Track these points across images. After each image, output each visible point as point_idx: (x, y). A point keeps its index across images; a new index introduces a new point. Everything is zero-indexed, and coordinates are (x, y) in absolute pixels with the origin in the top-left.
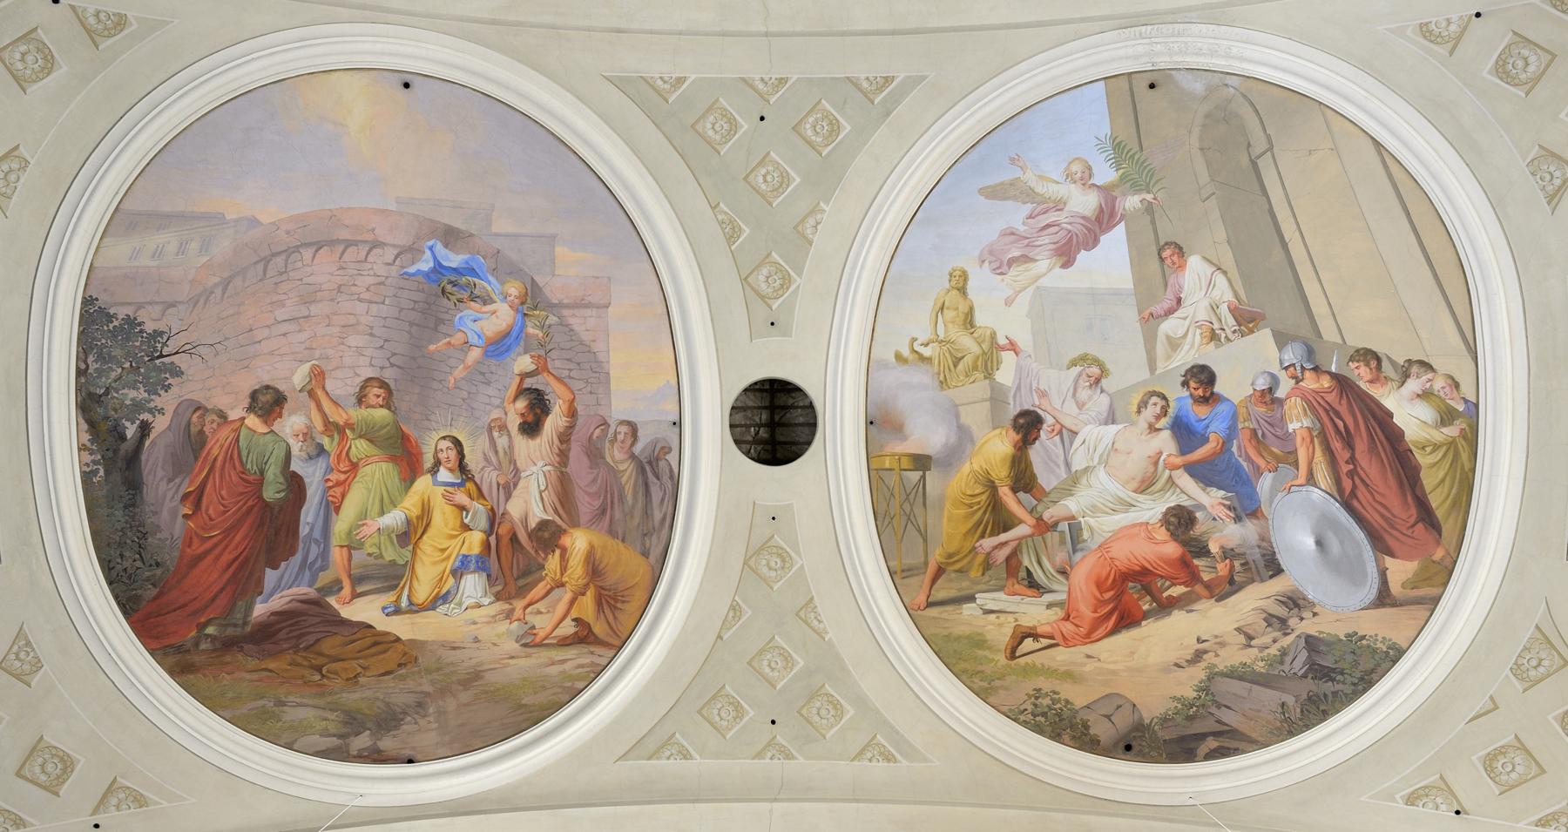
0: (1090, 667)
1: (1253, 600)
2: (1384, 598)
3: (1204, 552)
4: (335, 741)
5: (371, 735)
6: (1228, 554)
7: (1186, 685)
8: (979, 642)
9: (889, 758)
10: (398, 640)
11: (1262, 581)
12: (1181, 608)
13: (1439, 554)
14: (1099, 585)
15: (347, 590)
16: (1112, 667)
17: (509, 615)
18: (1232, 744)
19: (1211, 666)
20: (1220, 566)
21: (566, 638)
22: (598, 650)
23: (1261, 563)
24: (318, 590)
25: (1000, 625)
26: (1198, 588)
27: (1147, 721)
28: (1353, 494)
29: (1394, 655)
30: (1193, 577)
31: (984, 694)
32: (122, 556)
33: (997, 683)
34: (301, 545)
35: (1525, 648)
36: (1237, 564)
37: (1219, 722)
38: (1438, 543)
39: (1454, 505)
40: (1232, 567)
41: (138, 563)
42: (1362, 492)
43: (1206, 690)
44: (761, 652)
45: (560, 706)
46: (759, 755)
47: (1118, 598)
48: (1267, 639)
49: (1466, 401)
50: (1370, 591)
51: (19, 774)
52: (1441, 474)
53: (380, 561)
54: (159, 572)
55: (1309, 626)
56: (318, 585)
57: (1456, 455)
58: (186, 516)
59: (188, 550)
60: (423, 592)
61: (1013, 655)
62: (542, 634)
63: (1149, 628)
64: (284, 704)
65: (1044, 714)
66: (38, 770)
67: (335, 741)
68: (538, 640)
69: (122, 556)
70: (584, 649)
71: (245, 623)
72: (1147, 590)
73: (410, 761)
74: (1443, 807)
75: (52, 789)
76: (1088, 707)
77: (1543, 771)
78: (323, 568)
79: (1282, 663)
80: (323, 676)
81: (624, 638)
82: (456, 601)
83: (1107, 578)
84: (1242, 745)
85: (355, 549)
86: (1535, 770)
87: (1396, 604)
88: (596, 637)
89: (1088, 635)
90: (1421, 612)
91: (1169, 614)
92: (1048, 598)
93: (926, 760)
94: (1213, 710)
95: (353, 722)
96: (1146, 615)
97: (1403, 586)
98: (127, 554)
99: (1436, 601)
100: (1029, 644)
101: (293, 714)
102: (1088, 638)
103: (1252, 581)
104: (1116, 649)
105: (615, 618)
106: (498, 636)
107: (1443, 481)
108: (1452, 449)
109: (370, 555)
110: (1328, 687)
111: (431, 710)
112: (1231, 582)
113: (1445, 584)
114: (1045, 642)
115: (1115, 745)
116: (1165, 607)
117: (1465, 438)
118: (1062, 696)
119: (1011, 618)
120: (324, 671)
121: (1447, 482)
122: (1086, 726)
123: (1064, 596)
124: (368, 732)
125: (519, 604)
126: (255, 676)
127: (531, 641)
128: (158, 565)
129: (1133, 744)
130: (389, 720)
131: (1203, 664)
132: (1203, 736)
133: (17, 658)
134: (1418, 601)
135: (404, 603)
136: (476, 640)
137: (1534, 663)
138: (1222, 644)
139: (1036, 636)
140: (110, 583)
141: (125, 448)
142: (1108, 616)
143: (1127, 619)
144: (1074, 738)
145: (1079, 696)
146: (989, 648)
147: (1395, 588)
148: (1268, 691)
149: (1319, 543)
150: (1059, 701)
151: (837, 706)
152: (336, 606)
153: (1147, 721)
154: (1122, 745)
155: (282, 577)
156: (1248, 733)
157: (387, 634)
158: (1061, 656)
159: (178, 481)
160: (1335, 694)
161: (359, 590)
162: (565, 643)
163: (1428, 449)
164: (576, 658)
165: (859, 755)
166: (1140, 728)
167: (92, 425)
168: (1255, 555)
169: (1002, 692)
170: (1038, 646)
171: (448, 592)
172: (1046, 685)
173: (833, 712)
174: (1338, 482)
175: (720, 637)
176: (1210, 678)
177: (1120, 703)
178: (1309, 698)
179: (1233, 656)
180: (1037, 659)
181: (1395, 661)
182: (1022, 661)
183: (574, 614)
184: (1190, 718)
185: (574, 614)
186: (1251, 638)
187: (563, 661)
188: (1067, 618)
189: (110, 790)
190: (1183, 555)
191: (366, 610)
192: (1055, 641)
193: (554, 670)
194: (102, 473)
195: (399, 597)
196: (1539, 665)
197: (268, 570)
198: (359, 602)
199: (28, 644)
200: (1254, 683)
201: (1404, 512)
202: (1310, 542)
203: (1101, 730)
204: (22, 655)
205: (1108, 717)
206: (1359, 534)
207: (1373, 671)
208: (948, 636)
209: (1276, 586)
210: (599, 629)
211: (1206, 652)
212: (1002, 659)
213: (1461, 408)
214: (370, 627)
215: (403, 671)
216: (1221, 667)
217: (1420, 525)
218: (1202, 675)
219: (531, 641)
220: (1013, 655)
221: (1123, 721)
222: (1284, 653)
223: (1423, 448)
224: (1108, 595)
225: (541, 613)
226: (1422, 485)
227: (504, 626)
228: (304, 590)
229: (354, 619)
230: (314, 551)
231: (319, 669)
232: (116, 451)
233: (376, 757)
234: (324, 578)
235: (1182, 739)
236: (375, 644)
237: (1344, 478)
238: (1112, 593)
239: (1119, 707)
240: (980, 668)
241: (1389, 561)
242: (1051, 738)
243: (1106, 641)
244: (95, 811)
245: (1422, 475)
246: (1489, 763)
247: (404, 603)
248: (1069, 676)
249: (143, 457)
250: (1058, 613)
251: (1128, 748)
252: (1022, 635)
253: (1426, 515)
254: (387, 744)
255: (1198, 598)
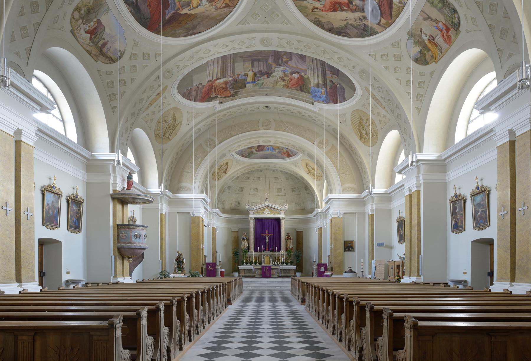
0: (326, 16)
1: (358, 15)
2: (379, 24)
3: (352, 4)
4: (186, 34)
5: (192, 31)
6: (356, 5)
7: (343, 24)
8: (306, 8)
9: (287, 24)
10: (192, 14)
11: (361, 12)
12: (345, 11)
13: (390, 22)
14: (331, 3)
15: (181, 9)
16: (331, 17)
17: (212, 5)
18: (347, 35)
19: (347, 22)
20: (354, 7)
21: (224, 7)
22: (230, 8)
23: (361, 9)
24: (176, 11)
25: (311, 5)
26: (349, 9)
27: (334, 27)
28: (381, 5)
29: (377, 33)
30: (349, 7)
31: (306, 16)
32: (142, 20)
33: (309, 15)
34: (170, 4)
35: (395, 42)
36: (357, 8)
37: (346, 31)
38: (391, 20)
39: (395, 16)
40: (356, 8)
41: (145, 20)
42: (382, 5)
43: (346, 26)
44: (263, 6)
45: (224, 18)
46: (263, 23)
47: (334, 6)
48: (358, 21)
49: (405, 2)
50: (377, 22)
51: (144, 59)
52: (396, 10)
53: (185, 2)
54: (148, 19)
55: (366, 22)
56: (175, 10)
57: (399, 9)
58: (149, 9)
59: (152, 14)
60: (195, 5)
61: (312, 11)
62: (219, 7)
63: (338, 13)
64: (176, 31)
65: (316, 22)
66: (145, 57)
67: (186, 34)
68: (218, 8)
69: (142, 20)
70: (227, 8)
71: (165, 21)
72: (340, 6)
73: (200, 33)
74: (373, 58)
75: (148, 59)
76: (324, 22)
77: (388, 60)
78: (175, 7)
79: (359, 26)
80: (181, 24)
81: (235, 5)
82: (202, 5)
83: (333, 2)
84: (349, 36)
85: (180, 2)
86: (387, 59)
87: (380, 25)
88: (230, 6)
89: (327, 11)
90: (384, 29)
91: (343, 11)
92: (321, 3)
93: (293, 25)
94: (346, 29)
95: (188, 30)
96: (338, 10)
97: (383, 23)
98: (142, 19)
99: (386, 28)
100: (316, 10)
101: (178, 32)
102: (327, 11)
103: (359, 12)
104: (332, 15)
105: (233, 2)
106: (211, 9)
107: (396, 11)
108: (399, 8)
109: (183, 2)
110: (365, 33)
111: (201, 24)
112: (355, 10)
113: (389, 27)
114: (319, 10)
115: (328, 29)
116: (342, 10)
117: (402, 7)
118: (320, 20)
119: (313, 5)
120: (181, 23)
121: (396, 12)
122: (323, 25)
123: (324, 3)
124: (191, 31)
125: (214, 3)
126: (170, 28)
127: (217, 8)
128: (148, 19)
129: (331, 30)
130: (194, 27)
131: (346, 21)
132: (343, 33)
133: (135, 43)
134: (384, 27)
135: (192, 8)
136: (207, 10)
137: (395, 45)
138: (351, 19)
139: (317, 9)
140: (142, 25)
141: (135, 4)
142: (332, 8)
143: (335, 10)
144: (321, 27)
145: (323, 20)
146: (308, 9)
147: (381, 23)
148: (355, 29)
149: (372, 10)
150: (320, 20)
151: (278, 15)
152: (180, 12)
153: (334, 27)
154: (329, 30)
155: (168, 11)
156: (350, 34)
157: (190, 14)
158: (321, 13)
159: (145, 4)
160: (366, 34)
161: (183, 8)
162: (224, 7)
163: (396, 5)
164: (226, 10)
165: (282, 23)
166: (333, 28)
167: (128, 4)
168: (361, 8)
169: (309, 16)
170: (317, 10)
171: (200, 4)
172: (318, 17)
173: (277, 16)
174: (379, 2)
175: (254, 3)
176: (347, 24)
177: (330, 23)
178: (362, 33)
179: (352, 22)
180: (317, 13)
181: (377, 34)
182: (314, 12)
183: (225, 2)
184: (342, 29)
185: (225, 2)
186: (356, 20)
187: (224, 11)
188: (324, 7)
189: (156, 54)
190: (348, 3)
191: (186, 11)
192: (320, 10)
193: (222, 12)
194: (133, 10)
195: (191, 7)
196: (395, 46)
197: (166, 11)
198: (184, 10)
199: (135, 41)
200: (354, 28)
201: (388, 12)
202: (371, 10)
203: (326, 26)
204: (135, 43)
205: (328, 25)
206: (379, 12)
207: (373, 34)
208: (300, 6)
209: (362, 14)
210: (230, 4)
211: (347, 20)
212: (310, 11)
213: (403, 3)
214: (187, 14)
215: (195, 19)
216: (349, 23)
217: (389, 16)
218: (346, 23)
219: (217, 8)
220: (312, 11)
221: (330, 26)
222: (360, 25)
223: (395, 5)
224: (332, 5)
225: (218, 3)
226: (392, 10)
227: (212, 7)
228: (173, 12)
229: (183, 13)
230: (173, 5)
231: (180, 23)
232: (134, 6)
233: (194, 34)
234: (176, 8)
235: (339, 32)
236: (189, 16)
237: (380, 2)
238: (333, 5)
239: (330, 24)
240: (306, 12)
241: (382, 18)
242: (317, 26)
243: (330, 13)
244: (156, 59)
245: (393, 8)
246: (382, 55)
247: (192, 8)
248: (322, 17)
249: (138, 4)
250: (323, 6)
251: (330, 31)
252: (315, 8)
253: (391, 15)
254: (195, 31)
255: (349, 11)
